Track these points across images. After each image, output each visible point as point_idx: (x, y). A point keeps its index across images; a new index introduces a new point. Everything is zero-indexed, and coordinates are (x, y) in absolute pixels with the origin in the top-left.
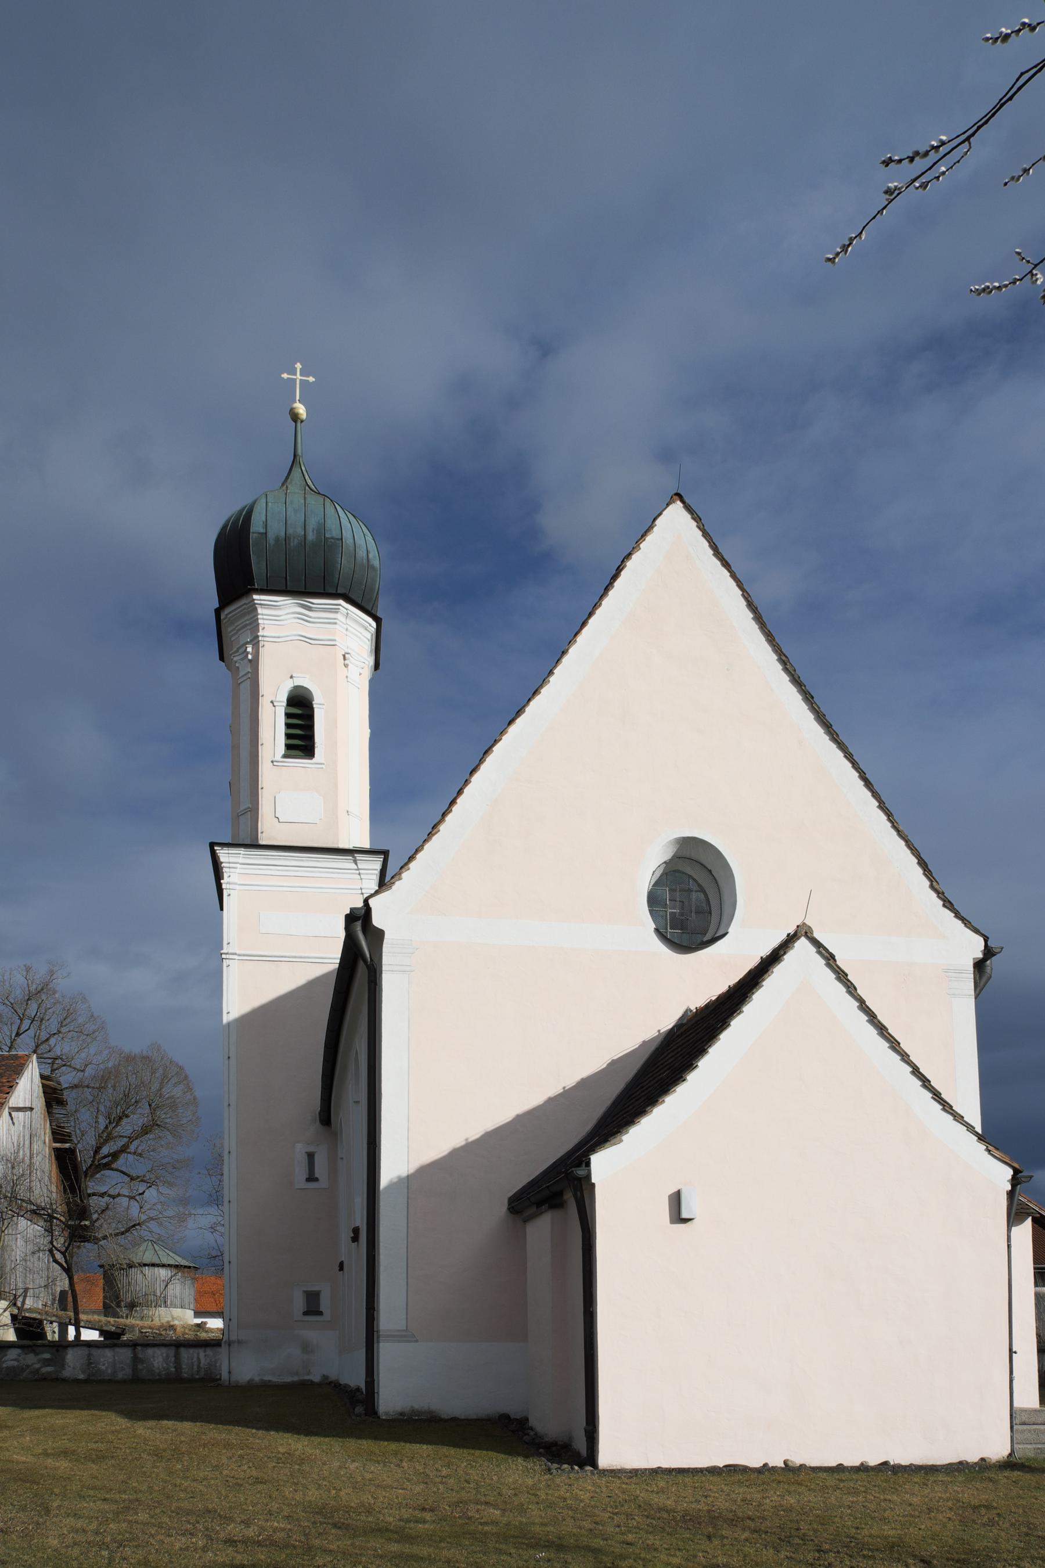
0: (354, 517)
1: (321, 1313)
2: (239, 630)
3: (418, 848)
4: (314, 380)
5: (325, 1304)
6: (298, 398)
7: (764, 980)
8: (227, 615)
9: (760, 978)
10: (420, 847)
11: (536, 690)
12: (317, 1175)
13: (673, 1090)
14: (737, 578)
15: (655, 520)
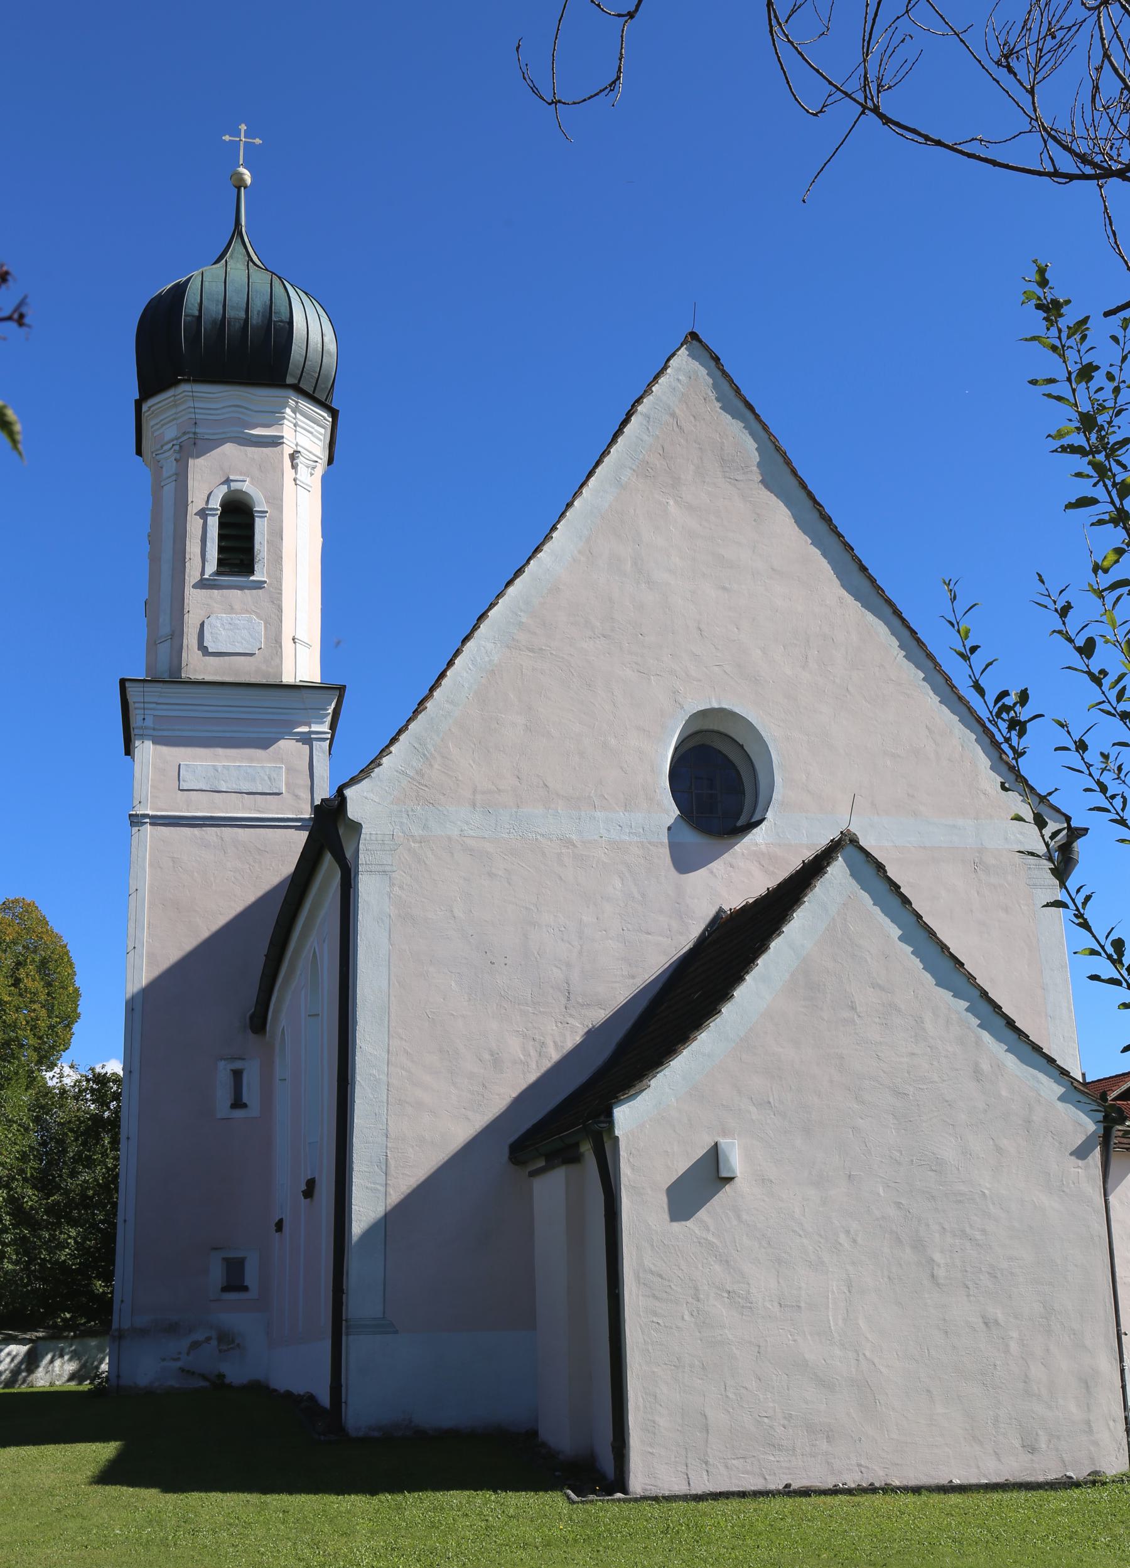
0: (306, 294)
1: (245, 1289)
2: (163, 425)
3: (402, 728)
4: (261, 142)
5: (251, 1277)
6: (241, 162)
7: (806, 895)
10: (404, 726)
11: (538, 548)
12: (245, 1099)
13: (705, 1024)
14: (762, 421)
15: (669, 360)
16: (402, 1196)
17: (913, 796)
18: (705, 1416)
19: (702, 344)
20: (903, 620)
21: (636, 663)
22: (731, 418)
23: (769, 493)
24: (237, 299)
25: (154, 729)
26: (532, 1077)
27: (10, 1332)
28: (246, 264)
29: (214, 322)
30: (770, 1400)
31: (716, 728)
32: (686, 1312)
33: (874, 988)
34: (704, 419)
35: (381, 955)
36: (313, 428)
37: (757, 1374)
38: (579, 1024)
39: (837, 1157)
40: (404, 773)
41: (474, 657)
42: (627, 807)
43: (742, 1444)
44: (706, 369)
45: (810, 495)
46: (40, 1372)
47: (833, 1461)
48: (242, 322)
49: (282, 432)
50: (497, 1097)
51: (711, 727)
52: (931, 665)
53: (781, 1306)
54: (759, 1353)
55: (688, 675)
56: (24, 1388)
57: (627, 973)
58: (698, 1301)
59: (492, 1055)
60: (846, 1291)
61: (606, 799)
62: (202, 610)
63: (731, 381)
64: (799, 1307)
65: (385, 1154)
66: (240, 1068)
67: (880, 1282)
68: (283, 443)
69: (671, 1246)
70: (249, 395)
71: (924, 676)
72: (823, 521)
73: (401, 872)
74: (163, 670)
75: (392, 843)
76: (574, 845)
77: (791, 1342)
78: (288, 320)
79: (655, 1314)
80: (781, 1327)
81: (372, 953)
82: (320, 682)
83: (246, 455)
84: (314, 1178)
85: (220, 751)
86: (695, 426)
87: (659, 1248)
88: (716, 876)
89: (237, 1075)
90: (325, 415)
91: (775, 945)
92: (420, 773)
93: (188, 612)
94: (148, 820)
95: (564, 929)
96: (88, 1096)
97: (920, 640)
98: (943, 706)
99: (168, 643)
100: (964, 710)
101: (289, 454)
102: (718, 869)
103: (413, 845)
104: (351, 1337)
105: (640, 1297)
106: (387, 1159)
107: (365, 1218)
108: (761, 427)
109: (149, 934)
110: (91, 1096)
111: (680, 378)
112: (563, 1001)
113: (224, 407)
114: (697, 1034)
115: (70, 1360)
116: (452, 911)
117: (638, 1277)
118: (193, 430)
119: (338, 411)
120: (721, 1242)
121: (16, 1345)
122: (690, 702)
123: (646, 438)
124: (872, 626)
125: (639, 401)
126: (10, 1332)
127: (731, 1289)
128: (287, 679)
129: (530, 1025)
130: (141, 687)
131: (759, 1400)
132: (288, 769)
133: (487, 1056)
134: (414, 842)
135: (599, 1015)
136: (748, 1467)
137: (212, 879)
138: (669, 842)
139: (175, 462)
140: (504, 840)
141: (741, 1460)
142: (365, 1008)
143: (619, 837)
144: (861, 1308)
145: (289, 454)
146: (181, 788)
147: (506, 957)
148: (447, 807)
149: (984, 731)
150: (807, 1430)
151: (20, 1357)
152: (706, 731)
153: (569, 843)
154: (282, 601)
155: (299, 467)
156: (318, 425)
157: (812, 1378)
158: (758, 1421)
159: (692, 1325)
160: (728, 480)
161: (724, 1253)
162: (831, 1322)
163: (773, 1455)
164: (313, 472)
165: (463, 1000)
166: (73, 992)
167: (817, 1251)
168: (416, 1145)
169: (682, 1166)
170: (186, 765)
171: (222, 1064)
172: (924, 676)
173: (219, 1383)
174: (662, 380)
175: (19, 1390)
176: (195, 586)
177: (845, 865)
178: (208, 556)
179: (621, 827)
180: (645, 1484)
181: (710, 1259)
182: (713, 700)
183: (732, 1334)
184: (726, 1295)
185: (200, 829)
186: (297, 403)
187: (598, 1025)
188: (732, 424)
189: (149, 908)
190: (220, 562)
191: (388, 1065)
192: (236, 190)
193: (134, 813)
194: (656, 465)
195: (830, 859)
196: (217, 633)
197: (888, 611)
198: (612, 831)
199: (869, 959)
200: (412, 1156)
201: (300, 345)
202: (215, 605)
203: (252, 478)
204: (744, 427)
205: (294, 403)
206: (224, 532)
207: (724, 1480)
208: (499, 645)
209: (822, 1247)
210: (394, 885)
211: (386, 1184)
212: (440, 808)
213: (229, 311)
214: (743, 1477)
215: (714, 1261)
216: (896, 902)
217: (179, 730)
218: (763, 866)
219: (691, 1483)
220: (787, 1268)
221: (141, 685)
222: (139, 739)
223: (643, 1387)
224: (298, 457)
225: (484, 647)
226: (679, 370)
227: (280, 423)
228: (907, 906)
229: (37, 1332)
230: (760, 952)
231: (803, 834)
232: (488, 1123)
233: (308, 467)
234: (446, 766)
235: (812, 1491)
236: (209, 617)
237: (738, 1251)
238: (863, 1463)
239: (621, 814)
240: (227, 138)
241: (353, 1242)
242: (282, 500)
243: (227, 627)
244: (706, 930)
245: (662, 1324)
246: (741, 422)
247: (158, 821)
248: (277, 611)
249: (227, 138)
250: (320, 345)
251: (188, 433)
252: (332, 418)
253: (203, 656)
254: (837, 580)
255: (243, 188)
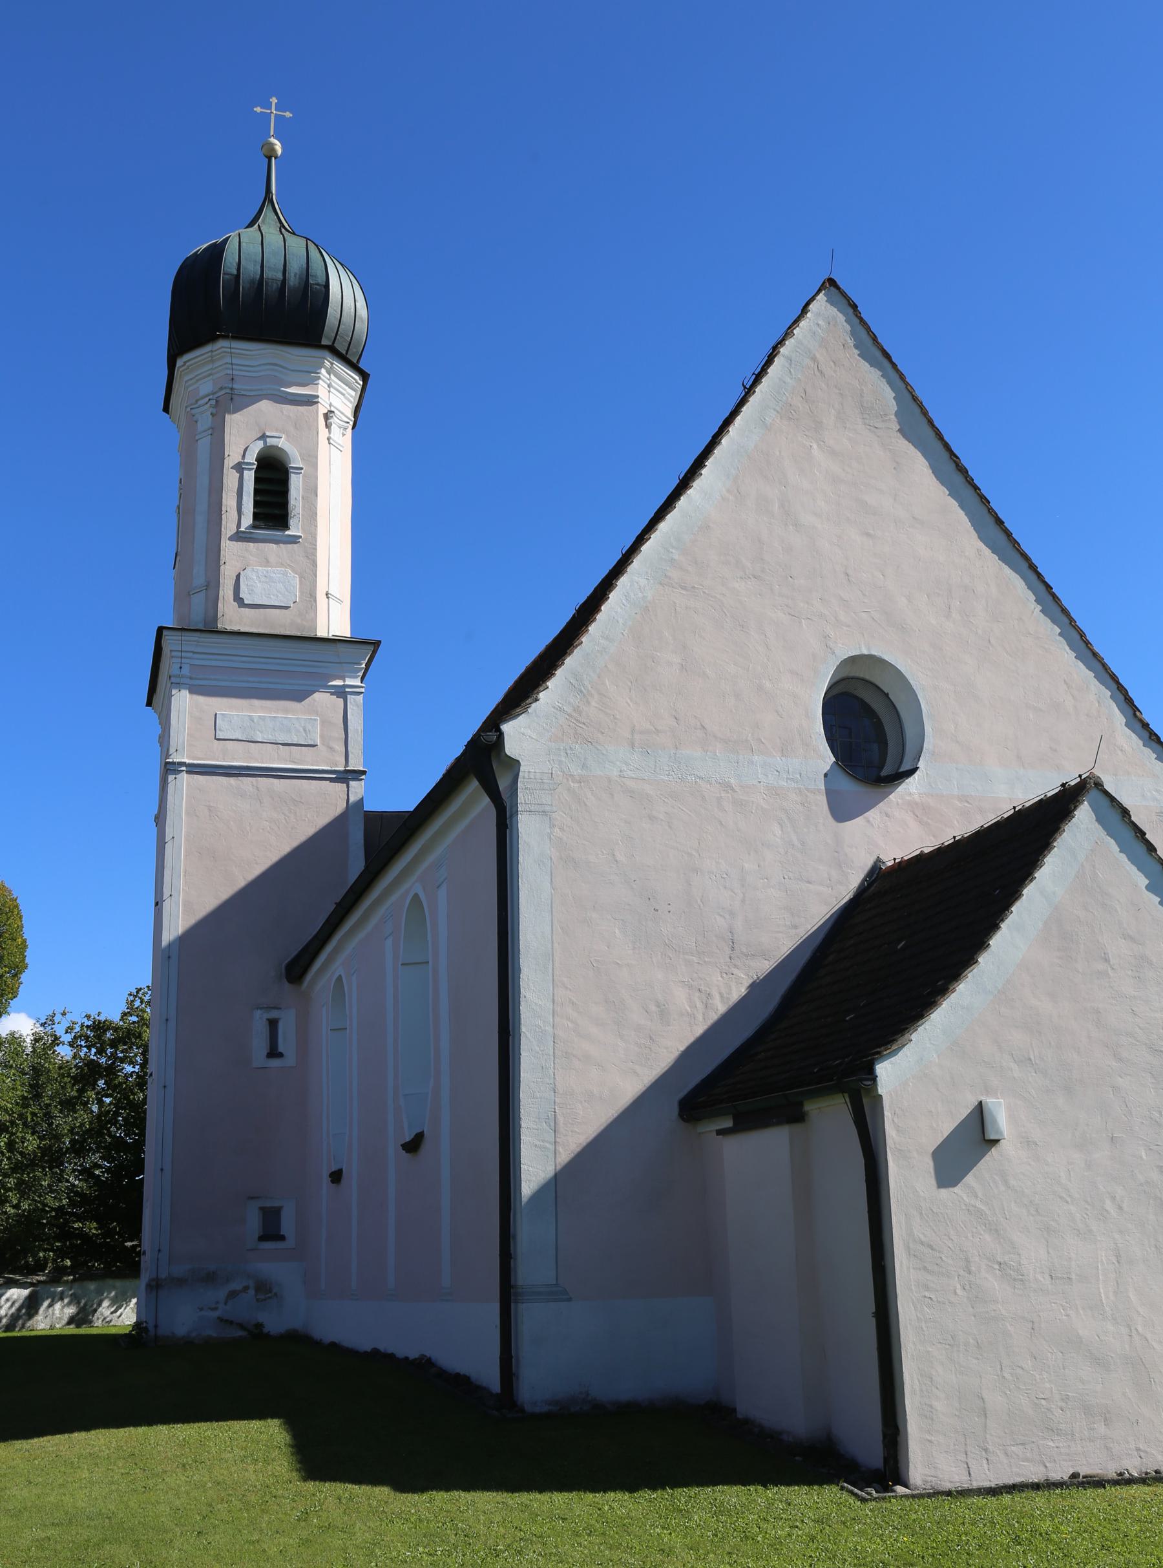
1: (282, 1238)
2: (197, 381)
5: (288, 1226)
6: (272, 133)
7: (1055, 840)
8: (185, 363)
9: (1051, 838)
12: (281, 1049)
13: (963, 975)
16: (572, 1155)
17: (1056, 750)
18: (983, 1399)
19: (840, 291)
20: (1039, 575)
21: (787, 606)
22: (869, 366)
23: (907, 442)
24: (274, 262)
25: (191, 678)
26: (699, 1030)
27: (11, 1276)
28: (279, 229)
29: (252, 281)
30: (1046, 1380)
31: (861, 675)
32: (958, 1286)
33: (1125, 939)
34: (843, 365)
35: (543, 900)
36: (345, 390)
37: (1032, 1353)
38: (744, 975)
39: (1099, 1118)
40: (561, 709)
41: (627, 593)
42: (784, 752)
43: (1021, 1429)
44: (844, 315)
45: (947, 447)
46: (39, 1317)
47: (1112, 1445)
48: (279, 283)
49: (317, 392)
50: (665, 1050)
51: (857, 674)
52: (1067, 621)
53: (1052, 1278)
54: (1033, 1329)
55: (837, 621)
56: (24, 1333)
57: (789, 923)
58: (970, 1273)
59: (658, 1007)
60: (1114, 1262)
61: (763, 743)
62: (238, 562)
63: (868, 329)
64: (1070, 1278)
65: (553, 1110)
66: (277, 1017)
67: (1147, 1251)
68: (318, 402)
69: (940, 1214)
70: (283, 353)
71: (1060, 631)
72: (959, 473)
73: (561, 813)
74: (197, 620)
75: (551, 782)
76: (733, 789)
77: (1064, 1317)
78: (324, 284)
79: (928, 1289)
80: (1054, 1301)
81: (534, 896)
82: (349, 636)
83: (282, 412)
84: (423, 1132)
85: (256, 702)
86: (835, 371)
87: (928, 1216)
88: (872, 825)
89: (273, 1024)
90: (357, 378)
91: (1029, 891)
92: (577, 710)
93: (225, 563)
94: (184, 768)
95: (726, 876)
96: (83, 1043)
97: (1056, 595)
98: (1079, 661)
99: (202, 594)
100: (1099, 666)
101: (324, 414)
102: (873, 818)
103: (572, 784)
104: (520, 1305)
105: (912, 1270)
106: (555, 1116)
107: (534, 1178)
108: (898, 376)
109: (185, 882)
110: (85, 1043)
111: (820, 323)
112: (728, 951)
113: (260, 365)
114: (956, 985)
115: (69, 1304)
116: (614, 855)
117: (909, 1247)
118: (230, 386)
119: (369, 375)
120: (990, 1209)
121: (18, 1288)
122: (840, 647)
123: (788, 380)
124: (1010, 579)
125: (781, 343)
126: (11, 1276)
127: (1002, 1261)
128: (321, 633)
129: (695, 975)
130: (179, 636)
131: (1036, 1380)
132: (323, 722)
133: (653, 1008)
134: (573, 782)
135: (764, 966)
136: (1028, 1455)
137: (248, 828)
138: (826, 789)
139: (211, 416)
140: (664, 782)
141: (1020, 1446)
142: (529, 956)
143: (777, 782)
144: (1130, 1280)
145: (324, 414)
146: (217, 737)
147: (669, 904)
148: (606, 747)
149: (1118, 687)
150: (1085, 1413)
151: (21, 1301)
152: (852, 678)
153: (729, 786)
154: (316, 557)
155: (332, 427)
156: (349, 388)
157: (1086, 1356)
158: (1036, 1403)
159: (965, 1300)
160: (868, 427)
161: (993, 1221)
162: (1102, 1295)
163: (1052, 1440)
164: (345, 433)
165: (627, 948)
166: (22, 944)
167: (1085, 1218)
168: (585, 1101)
169: (947, 1127)
170: (223, 714)
171: (258, 1013)
172: (1060, 631)
173: (257, 1333)
174: (802, 323)
175: (19, 1334)
176: (231, 539)
177: (1090, 809)
178: (244, 509)
179: (779, 772)
180: (925, 1475)
181: (979, 1228)
182: (863, 646)
183: (1006, 1309)
184: (997, 1267)
185: (236, 778)
186: (332, 364)
187: (763, 976)
188: (870, 372)
189: (186, 856)
190: (256, 516)
191: (553, 1016)
192: (267, 160)
193: (171, 760)
194: (799, 408)
195: (1077, 802)
196: (252, 586)
197: (1025, 565)
198: (770, 776)
199: (1119, 909)
200: (581, 1113)
201: (335, 308)
202: (251, 558)
203: (288, 436)
204: (882, 376)
205: (329, 364)
206: (260, 487)
207: (1005, 1469)
208: (652, 581)
209: (1090, 1215)
210: (554, 826)
211: (555, 1142)
212: (599, 747)
213: (267, 271)
214: (1023, 1465)
215: (984, 1231)
216: (1141, 849)
217: (215, 680)
218: (917, 817)
219: (972, 1473)
220: (1056, 1237)
221: (179, 633)
222: (176, 688)
223: (919, 1368)
224: (332, 417)
225: (637, 583)
226: (818, 315)
227: (315, 382)
228: (1153, 854)
229: (38, 1275)
230: (1014, 898)
231: (954, 785)
232: (656, 1078)
233: (340, 428)
234: (603, 703)
235: (1105, 1481)
236: (245, 569)
237: (1007, 1219)
238: (1141, 1447)
239: (778, 758)
240: (258, 109)
241: (523, 1204)
242: (316, 457)
243: (263, 579)
244: (865, 880)
245: (934, 1299)
246: (879, 370)
247: (194, 769)
248: (312, 566)
249: (258, 109)
250: (353, 310)
251: (225, 388)
252: (363, 381)
253: (239, 607)
254: (975, 533)
255: (273, 158)
